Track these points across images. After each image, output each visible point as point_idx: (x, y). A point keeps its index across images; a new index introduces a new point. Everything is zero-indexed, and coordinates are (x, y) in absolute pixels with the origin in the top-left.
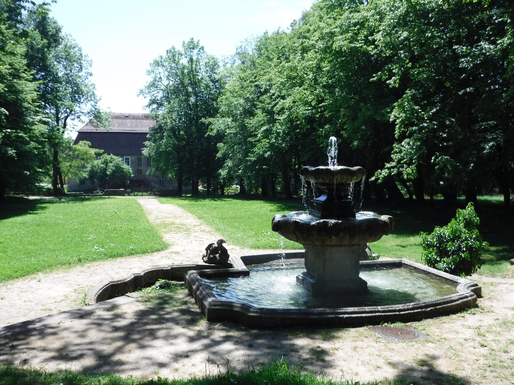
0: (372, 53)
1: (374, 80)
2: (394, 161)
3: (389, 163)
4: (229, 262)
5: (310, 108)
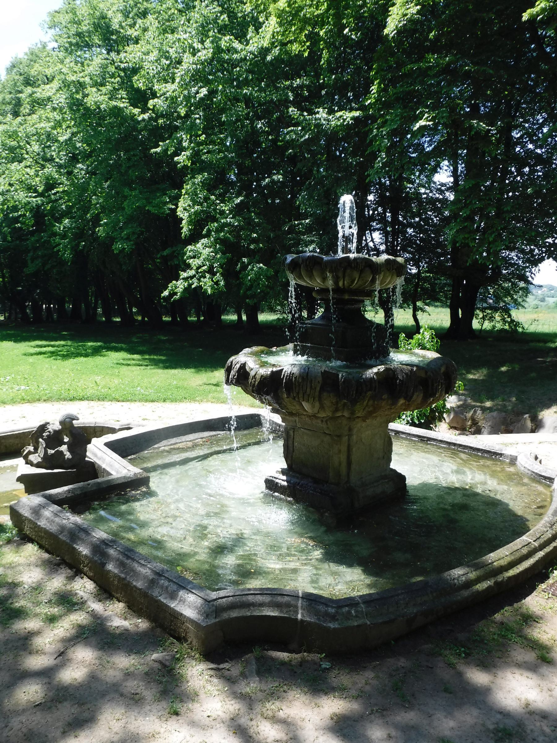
0: (140, 118)
1: (156, 153)
2: (192, 269)
3: (185, 271)
4: (87, 459)
5: (34, 195)
